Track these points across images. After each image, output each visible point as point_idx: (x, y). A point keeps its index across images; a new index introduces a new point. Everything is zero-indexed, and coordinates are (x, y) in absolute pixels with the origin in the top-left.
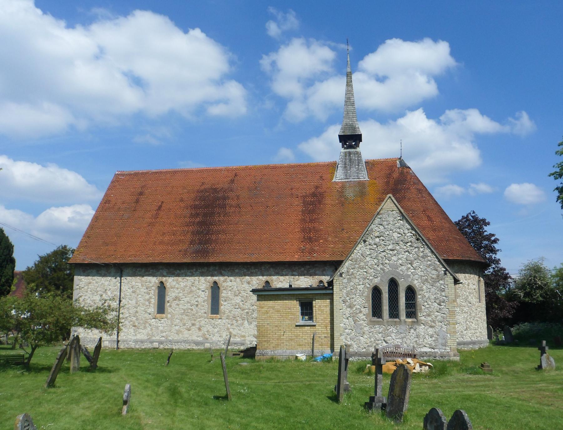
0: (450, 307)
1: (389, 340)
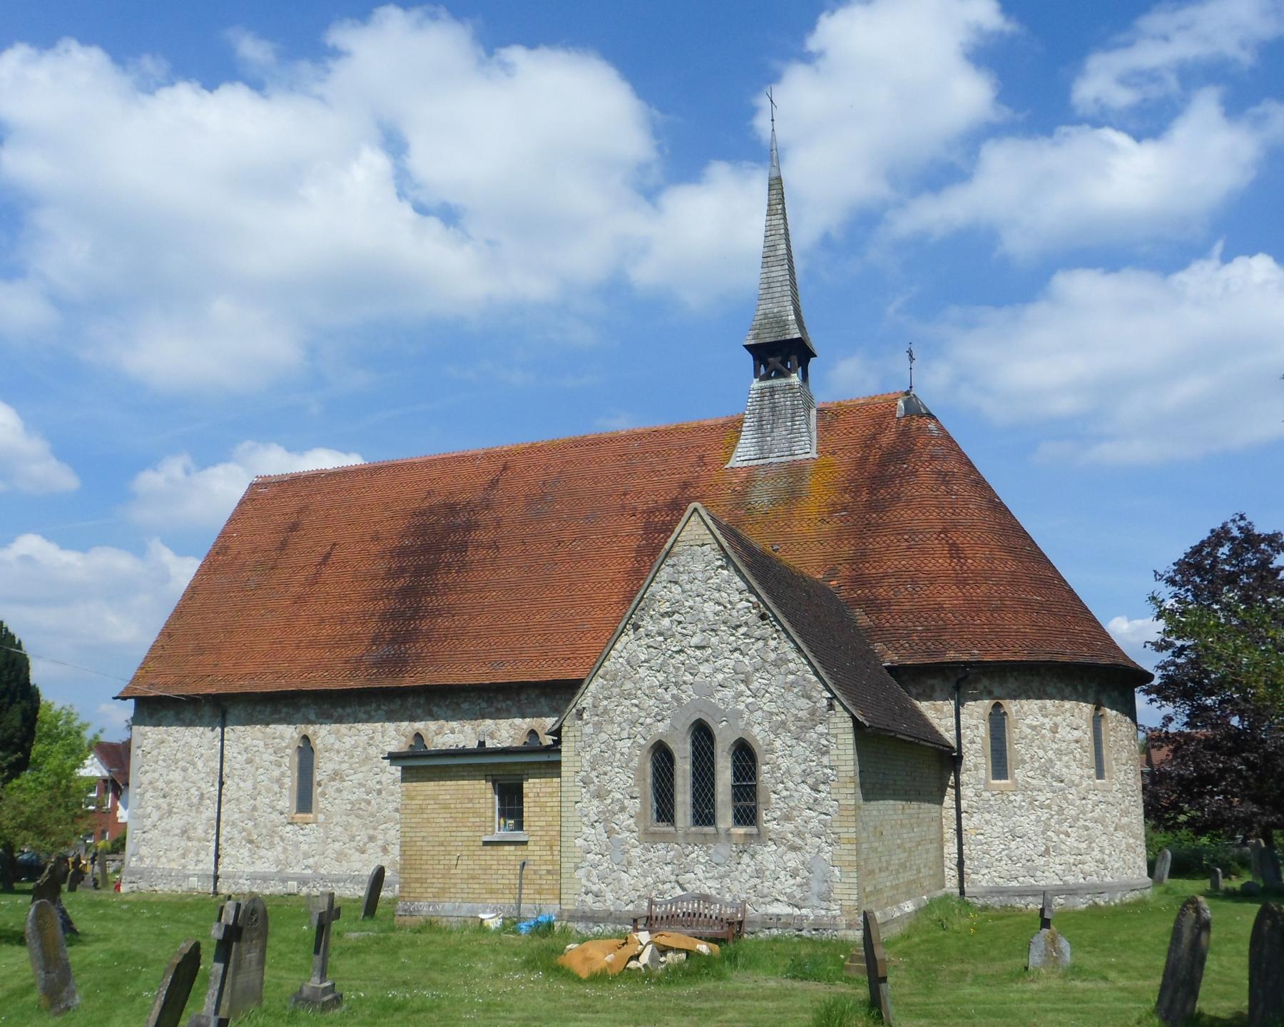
0: (843, 796)
1: (689, 883)
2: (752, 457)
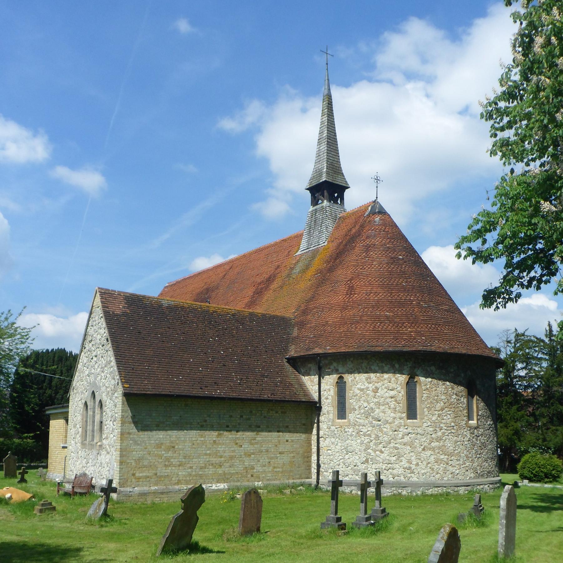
2: (305, 249)
